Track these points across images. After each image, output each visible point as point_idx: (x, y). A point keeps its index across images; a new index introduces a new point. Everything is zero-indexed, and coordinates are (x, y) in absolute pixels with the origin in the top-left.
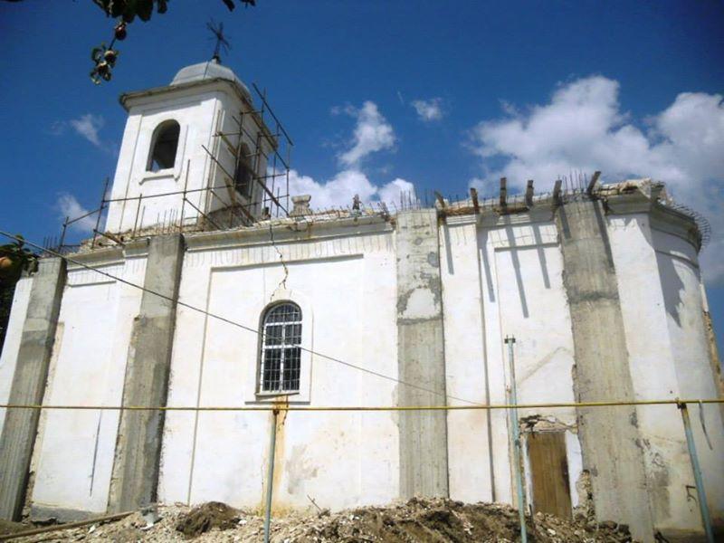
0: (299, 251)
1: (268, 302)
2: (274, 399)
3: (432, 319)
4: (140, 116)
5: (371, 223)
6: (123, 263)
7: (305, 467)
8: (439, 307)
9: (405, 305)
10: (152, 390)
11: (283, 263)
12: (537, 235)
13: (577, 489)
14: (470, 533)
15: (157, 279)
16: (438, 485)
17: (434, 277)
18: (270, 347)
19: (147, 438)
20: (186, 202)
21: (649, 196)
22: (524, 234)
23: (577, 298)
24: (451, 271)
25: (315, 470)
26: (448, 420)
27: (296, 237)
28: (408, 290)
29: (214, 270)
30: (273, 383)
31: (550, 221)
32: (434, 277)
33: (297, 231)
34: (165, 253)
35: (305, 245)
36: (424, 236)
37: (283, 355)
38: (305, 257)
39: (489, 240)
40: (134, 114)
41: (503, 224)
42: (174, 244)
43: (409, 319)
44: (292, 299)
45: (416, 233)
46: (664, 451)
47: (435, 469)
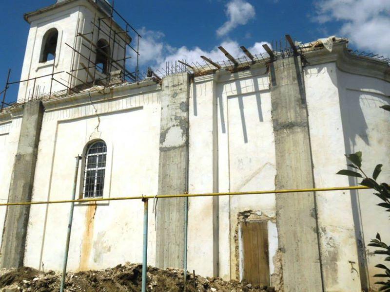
0: (107, 107)
1: (88, 141)
2: (88, 203)
3: (180, 147)
4: (36, 27)
5: (148, 86)
6: (11, 122)
7: (104, 245)
8: (184, 138)
9: (165, 138)
10: (22, 199)
11: (98, 115)
12: (256, 85)
13: (274, 262)
14: (152, 288)
15: (26, 130)
16: (178, 257)
17: (183, 118)
18: (89, 169)
19: (18, 229)
20: (53, 80)
21: (331, 50)
22: (247, 85)
23: (281, 127)
24: (196, 114)
25: (110, 247)
26: (189, 214)
27: (105, 98)
28: (167, 128)
29: (59, 122)
30: (90, 192)
31: (265, 74)
32: (183, 118)
33: (105, 94)
34: (31, 114)
35: (110, 103)
36: (178, 91)
37: (96, 174)
38: (110, 111)
39: (224, 91)
40: (33, 27)
41: (233, 79)
42: (36, 108)
43: (166, 148)
44: (101, 138)
45: (174, 90)
46: (336, 236)
47: (177, 247)
